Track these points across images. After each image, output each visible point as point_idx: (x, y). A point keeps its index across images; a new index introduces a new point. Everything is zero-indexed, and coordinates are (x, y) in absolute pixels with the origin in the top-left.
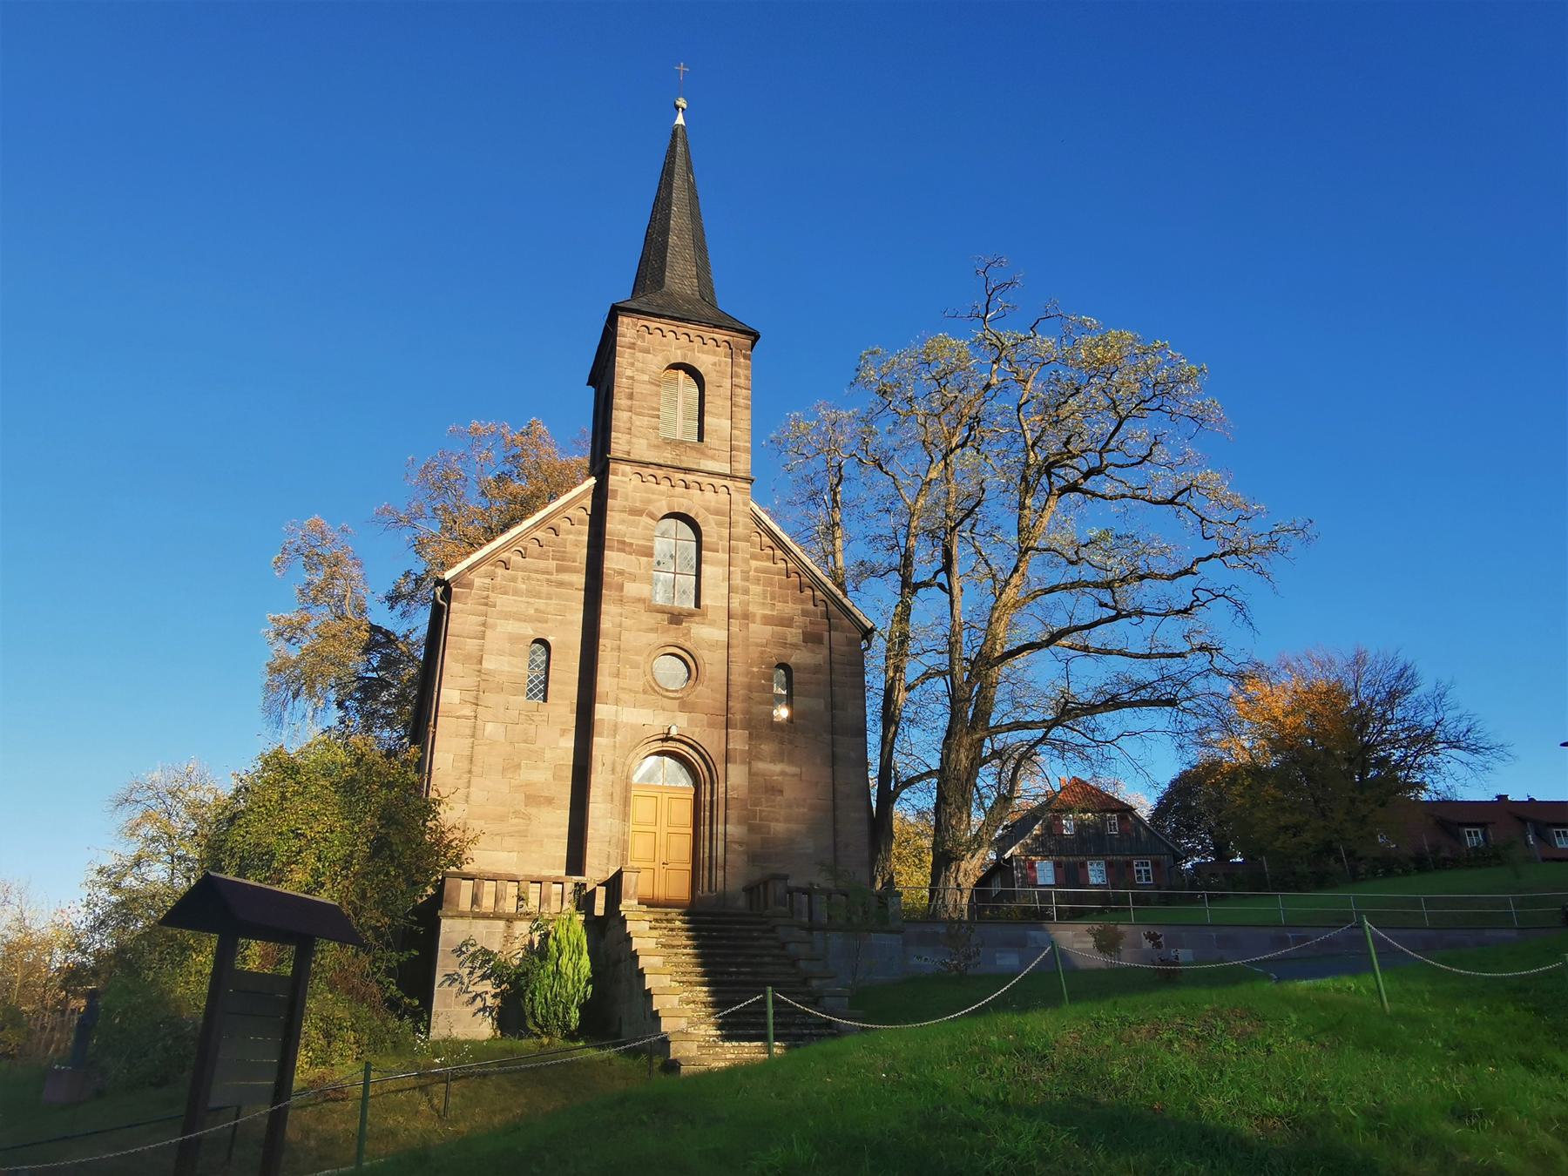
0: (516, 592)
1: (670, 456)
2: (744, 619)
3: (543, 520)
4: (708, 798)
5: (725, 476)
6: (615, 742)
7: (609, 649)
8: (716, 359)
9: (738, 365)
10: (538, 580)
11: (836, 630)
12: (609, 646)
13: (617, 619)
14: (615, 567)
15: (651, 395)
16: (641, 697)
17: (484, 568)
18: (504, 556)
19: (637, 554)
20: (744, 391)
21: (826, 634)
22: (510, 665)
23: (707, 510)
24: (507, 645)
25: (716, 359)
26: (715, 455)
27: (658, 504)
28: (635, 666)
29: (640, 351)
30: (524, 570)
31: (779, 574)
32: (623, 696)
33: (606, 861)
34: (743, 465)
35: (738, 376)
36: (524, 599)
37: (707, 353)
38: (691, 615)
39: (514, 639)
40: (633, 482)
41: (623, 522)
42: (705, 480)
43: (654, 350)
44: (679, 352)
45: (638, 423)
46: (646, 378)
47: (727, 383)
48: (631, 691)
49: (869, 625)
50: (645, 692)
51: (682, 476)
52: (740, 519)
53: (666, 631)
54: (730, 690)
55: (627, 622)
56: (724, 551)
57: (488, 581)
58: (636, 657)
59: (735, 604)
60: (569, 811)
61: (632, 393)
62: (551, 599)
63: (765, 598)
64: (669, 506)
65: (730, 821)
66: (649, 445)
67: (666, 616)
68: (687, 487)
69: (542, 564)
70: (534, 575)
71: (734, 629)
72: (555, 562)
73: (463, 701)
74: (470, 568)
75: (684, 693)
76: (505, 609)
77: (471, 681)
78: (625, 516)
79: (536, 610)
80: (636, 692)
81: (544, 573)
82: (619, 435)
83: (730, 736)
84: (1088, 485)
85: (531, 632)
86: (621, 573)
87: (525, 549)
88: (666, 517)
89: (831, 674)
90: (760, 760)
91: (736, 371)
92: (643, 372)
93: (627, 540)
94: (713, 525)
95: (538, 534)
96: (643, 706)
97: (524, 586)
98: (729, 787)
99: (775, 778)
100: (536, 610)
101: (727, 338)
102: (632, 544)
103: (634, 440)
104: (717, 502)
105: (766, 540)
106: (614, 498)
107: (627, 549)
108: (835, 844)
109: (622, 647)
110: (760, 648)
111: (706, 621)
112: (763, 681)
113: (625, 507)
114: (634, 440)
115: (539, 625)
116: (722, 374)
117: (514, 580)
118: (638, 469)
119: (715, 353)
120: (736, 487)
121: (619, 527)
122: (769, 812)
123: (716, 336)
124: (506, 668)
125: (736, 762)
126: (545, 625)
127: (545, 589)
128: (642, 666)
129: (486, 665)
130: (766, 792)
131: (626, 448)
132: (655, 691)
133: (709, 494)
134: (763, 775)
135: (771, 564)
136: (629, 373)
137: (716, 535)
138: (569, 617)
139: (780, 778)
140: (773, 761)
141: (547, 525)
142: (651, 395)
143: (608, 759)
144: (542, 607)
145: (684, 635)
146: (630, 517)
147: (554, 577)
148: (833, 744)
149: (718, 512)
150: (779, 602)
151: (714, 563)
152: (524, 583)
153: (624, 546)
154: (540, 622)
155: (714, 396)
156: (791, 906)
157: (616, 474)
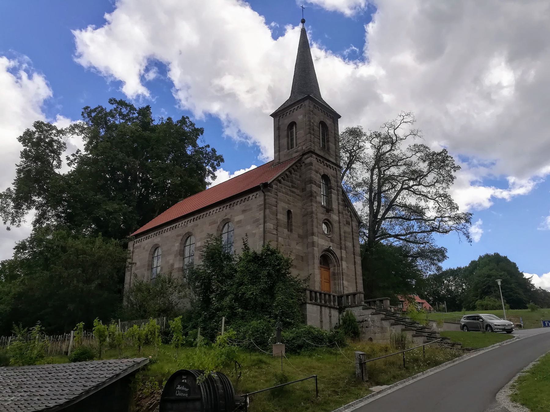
17: (275, 182)
21: (351, 222)
23: (332, 175)
39: (284, 209)
42: (332, 165)
85: (286, 206)
103: (315, 146)
115: (289, 205)
118: (317, 157)
127: (289, 193)
129: (278, 217)
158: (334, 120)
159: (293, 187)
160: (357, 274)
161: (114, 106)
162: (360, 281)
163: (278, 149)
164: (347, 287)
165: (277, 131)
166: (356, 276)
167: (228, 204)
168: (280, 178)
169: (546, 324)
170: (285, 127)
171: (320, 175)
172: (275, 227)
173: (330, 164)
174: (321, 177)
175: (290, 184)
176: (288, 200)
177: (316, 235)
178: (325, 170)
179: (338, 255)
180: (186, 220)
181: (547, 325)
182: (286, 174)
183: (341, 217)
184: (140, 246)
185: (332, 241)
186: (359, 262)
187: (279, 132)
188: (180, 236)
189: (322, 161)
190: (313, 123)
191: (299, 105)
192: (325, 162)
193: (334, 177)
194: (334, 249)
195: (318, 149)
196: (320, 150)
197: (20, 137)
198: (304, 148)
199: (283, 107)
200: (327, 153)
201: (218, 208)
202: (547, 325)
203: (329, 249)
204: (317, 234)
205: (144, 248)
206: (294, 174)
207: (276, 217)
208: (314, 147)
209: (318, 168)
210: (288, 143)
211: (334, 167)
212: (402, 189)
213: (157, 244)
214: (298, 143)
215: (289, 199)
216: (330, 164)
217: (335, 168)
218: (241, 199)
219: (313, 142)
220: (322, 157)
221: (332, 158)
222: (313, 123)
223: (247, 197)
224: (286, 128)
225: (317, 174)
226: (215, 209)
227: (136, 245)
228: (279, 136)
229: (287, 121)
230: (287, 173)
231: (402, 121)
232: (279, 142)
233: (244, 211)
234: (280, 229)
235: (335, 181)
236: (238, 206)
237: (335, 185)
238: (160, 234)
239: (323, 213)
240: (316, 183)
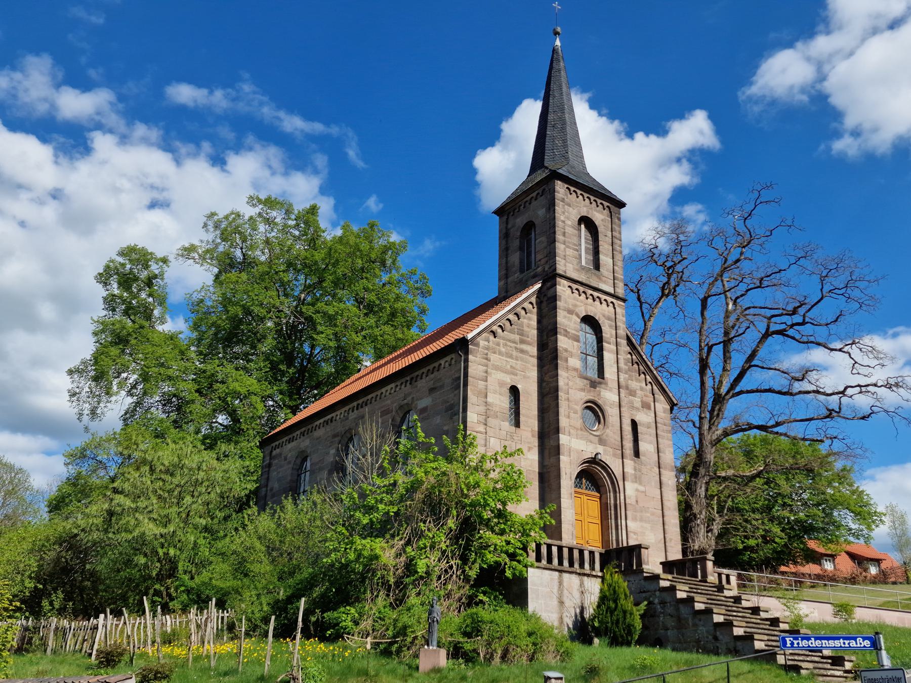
0: (500, 353)
4: (612, 502)
17: (484, 335)
21: (652, 404)
22: (502, 401)
23: (604, 316)
24: (498, 388)
27: (580, 308)
30: (504, 339)
36: (504, 358)
37: (598, 212)
39: (501, 384)
41: (565, 317)
42: (603, 297)
47: (609, 234)
49: (675, 402)
50: (581, 430)
57: (486, 343)
60: (538, 502)
68: (594, 300)
70: (509, 344)
73: (479, 422)
74: (479, 334)
76: (496, 364)
77: (482, 409)
83: (625, 464)
84: (791, 332)
85: (509, 381)
86: (566, 350)
93: (568, 330)
103: (567, 264)
106: (560, 301)
115: (513, 377)
117: (498, 345)
118: (571, 284)
119: (602, 213)
123: (604, 202)
124: (498, 402)
126: (516, 377)
127: (515, 353)
129: (489, 400)
131: (564, 269)
136: (562, 218)
138: (528, 374)
143: (568, 471)
147: (519, 346)
154: (513, 374)
156: (588, 575)
157: (560, 285)
158: (611, 212)
159: (522, 342)
160: (664, 507)
161: (257, 210)
162: (672, 521)
163: (504, 272)
164: (635, 533)
165: (504, 242)
166: (662, 510)
167: (408, 378)
168: (495, 328)
169: (788, 642)
170: (516, 233)
171: (577, 315)
172: (482, 418)
173: (600, 296)
174: (579, 320)
175: (517, 337)
176: (511, 366)
177: (567, 433)
178: (589, 308)
179: (617, 471)
180: (347, 408)
181: (789, 645)
182: (508, 319)
183: (622, 395)
184: (280, 454)
185: (602, 442)
186: (670, 483)
187: (507, 241)
188: (338, 436)
189: (581, 291)
190: (564, 222)
191: (540, 191)
192: (590, 292)
193: (609, 319)
194: (608, 457)
195: (574, 269)
196: (578, 270)
197: (100, 274)
198: (546, 269)
199: (514, 196)
200: (595, 274)
201: (393, 385)
202: (789, 645)
203: (595, 458)
204: (567, 429)
205: (285, 459)
206: (525, 318)
207: (484, 400)
208: (565, 265)
209: (572, 305)
210: (521, 262)
211: (610, 299)
212: (767, 335)
213: (303, 452)
214: (537, 259)
215: (514, 365)
216: (600, 296)
217: (612, 302)
218: (427, 368)
219: (562, 257)
220: (582, 284)
221: (605, 282)
222: (564, 222)
223: (436, 364)
224: (519, 234)
225: (570, 316)
226: (389, 387)
227: (274, 453)
228: (507, 249)
229: (520, 221)
230: (511, 317)
231: (758, 202)
232: (507, 260)
233: (432, 390)
234: (491, 421)
235: (610, 326)
236: (424, 380)
237: (611, 334)
238: (310, 434)
239: (583, 390)
240: (569, 332)
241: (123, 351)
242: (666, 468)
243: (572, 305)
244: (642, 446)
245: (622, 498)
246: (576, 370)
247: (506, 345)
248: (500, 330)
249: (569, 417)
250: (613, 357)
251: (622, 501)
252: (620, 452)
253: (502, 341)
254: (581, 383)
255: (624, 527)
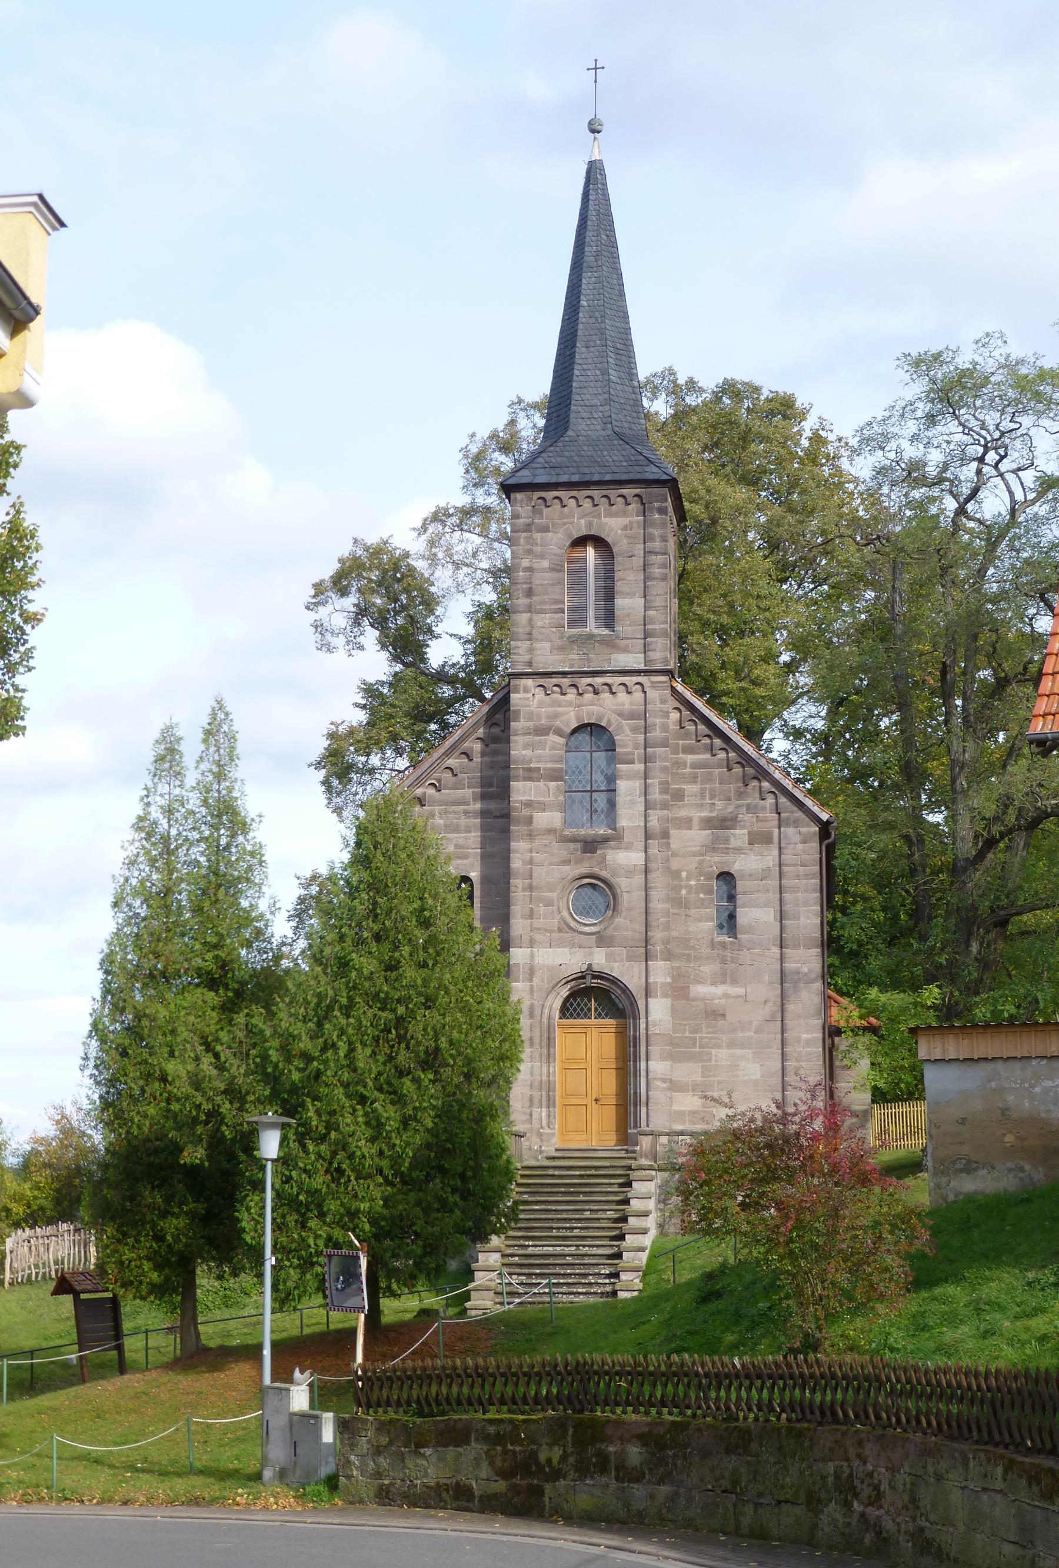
1: (576, 657)
2: (663, 838)
3: (454, 747)
5: (638, 672)
6: (532, 986)
7: (520, 889)
8: (626, 521)
9: (653, 524)
10: (455, 813)
11: (788, 825)
12: (520, 886)
13: (527, 856)
14: (521, 798)
15: (552, 585)
16: (556, 935)
18: (419, 791)
19: (545, 780)
20: (659, 557)
21: (776, 831)
23: (620, 714)
25: (626, 521)
26: (627, 645)
27: (565, 718)
28: (549, 903)
29: (538, 531)
31: (719, 766)
32: (538, 937)
33: (528, 1104)
34: (663, 654)
35: (653, 540)
38: (606, 840)
40: (537, 696)
41: (526, 746)
43: (554, 525)
44: (582, 521)
45: (539, 624)
46: (546, 564)
47: (639, 550)
48: (546, 930)
50: (560, 930)
51: (589, 680)
52: (658, 721)
53: (580, 861)
54: (650, 919)
55: (538, 857)
56: (640, 762)
58: (549, 894)
59: (654, 822)
61: (531, 588)
62: (470, 832)
63: (703, 797)
64: (578, 718)
65: (651, 1056)
66: (553, 648)
67: (579, 845)
68: (596, 692)
69: (459, 793)
71: (653, 851)
72: (471, 790)
75: (602, 927)
78: (528, 738)
79: (457, 846)
80: (551, 931)
81: (459, 804)
82: (519, 643)
83: (650, 969)
86: (529, 804)
87: (439, 781)
88: (575, 731)
89: (780, 880)
90: (700, 983)
91: (650, 533)
92: (542, 557)
94: (628, 731)
95: (451, 762)
96: (559, 946)
97: (442, 822)
98: (650, 1023)
99: (716, 1001)
100: (457, 846)
101: (637, 491)
102: (539, 769)
103: (537, 645)
104: (632, 704)
105: (702, 727)
107: (535, 775)
108: (783, 1069)
109: (534, 884)
110: (697, 858)
111: (623, 845)
112: (702, 896)
113: (528, 728)
114: (537, 645)
116: (632, 539)
118: (541, 681)
119: (625, 514)
120: (652, 682)
121: (524, 752)
122: (712, 1038)
125: (656, 996)
128: (556, 902)
130: (707, 1017)
131: (527, 658)
132: (570, 928)
133: (622, 696)
134: (703, 999)
135: (708, 756)
137: (630, 743)
139: (723, 1001)
140: (714, 983)
141: (460, 751)
142: (552, 585)
144: (461, 842)
145: (599, 863)
146: (537, 738)
148: (782, 959)
149: (632, 716)
150: (720, 800)
151: (629, 777)
152: (441, 818)
153: (531, 774)
155: (625, 570)
157: (517, 691)
221: (626, 650)
239: (566, 862)
241: (170, 794)
242: (796, 946)
243: (548, 717)
244: (745, 916)
245: (643, 1026)
246: (550, 831)
247: (446, 812)
248: (431, 791)
249: (531, 915)
250: (637, 784)
251: (643, 1031)
252: (643, 950)
253: (437, 809)
254: (561, 851)
255: (643, 1073)
